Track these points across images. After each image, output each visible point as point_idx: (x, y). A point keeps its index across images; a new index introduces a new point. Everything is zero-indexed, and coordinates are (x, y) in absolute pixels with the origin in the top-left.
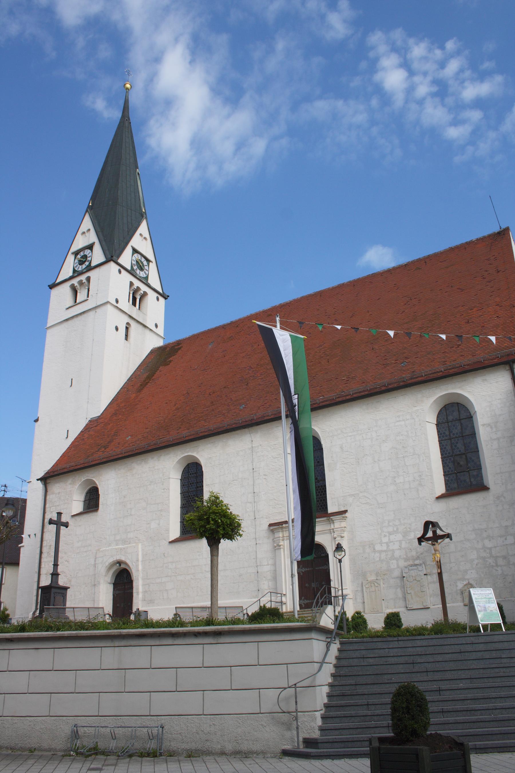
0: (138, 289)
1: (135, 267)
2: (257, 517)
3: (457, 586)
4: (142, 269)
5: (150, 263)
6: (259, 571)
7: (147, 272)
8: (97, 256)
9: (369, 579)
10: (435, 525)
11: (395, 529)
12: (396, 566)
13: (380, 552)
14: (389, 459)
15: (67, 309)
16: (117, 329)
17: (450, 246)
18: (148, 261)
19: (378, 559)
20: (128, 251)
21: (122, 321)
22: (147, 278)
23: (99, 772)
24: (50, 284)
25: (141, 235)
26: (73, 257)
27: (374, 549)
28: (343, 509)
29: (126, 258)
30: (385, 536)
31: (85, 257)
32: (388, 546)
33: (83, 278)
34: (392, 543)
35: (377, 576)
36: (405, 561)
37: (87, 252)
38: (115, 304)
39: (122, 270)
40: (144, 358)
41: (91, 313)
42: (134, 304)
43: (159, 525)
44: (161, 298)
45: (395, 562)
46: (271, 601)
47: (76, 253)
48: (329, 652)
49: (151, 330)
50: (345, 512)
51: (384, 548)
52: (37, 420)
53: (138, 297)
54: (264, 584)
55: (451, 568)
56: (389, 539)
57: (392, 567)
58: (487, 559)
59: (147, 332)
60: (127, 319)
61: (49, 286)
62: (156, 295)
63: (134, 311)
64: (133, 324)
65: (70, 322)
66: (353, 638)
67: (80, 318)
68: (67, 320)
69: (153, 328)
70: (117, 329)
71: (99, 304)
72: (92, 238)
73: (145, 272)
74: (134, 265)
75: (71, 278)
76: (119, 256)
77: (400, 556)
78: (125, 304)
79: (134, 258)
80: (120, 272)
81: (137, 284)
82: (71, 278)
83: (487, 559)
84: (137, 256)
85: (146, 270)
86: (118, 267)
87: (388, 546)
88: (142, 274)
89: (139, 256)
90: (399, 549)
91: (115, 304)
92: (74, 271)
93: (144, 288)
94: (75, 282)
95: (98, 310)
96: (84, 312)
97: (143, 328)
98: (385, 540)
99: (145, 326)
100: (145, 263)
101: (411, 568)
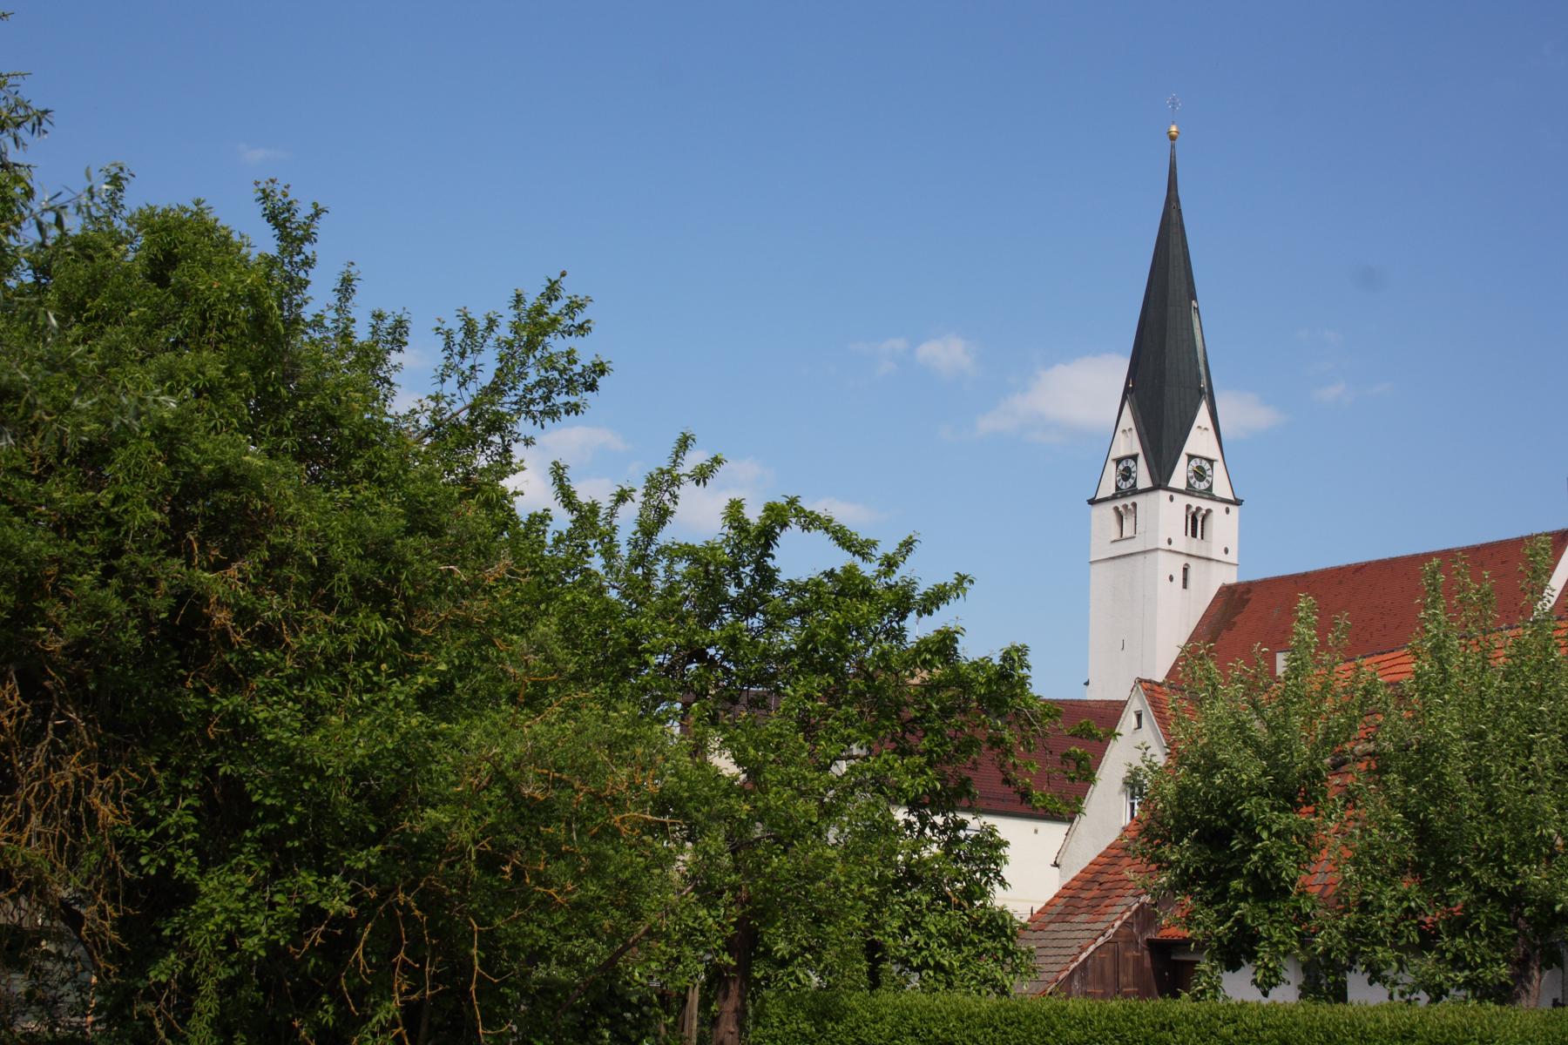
0: (1198, 509)
8: (1143, 479)
16: (1171, 578)
20: (1183, 459)
21: (1176, 565)
23: (568, 473)
26: (1114, 465)
29: (1179, 479)
31: (1127, 469)
33: (1128, 501)
37: (1131, 463)
38: (1167, 547)
41: (1140, 557)
42: (1194, 535)
44: (1232, 508)
47: (1118, 461)
48: (355, 298)
63: (1195, 546)
64: (1193, 563)
66: (1083, 949)
67: (1128, 560)
69: (1222, 557)
70: (1171, 578)
72: (1136, 448)
75: (1114, 497)
76: (1168, 480)
78: (1182, 542)
82: (1114, 497)
92: (1117, 488)
93: (1205, 504)
94: (1119, 504)
95: (1149, 556)
99: (1209, 559)
100: (1206, 466)
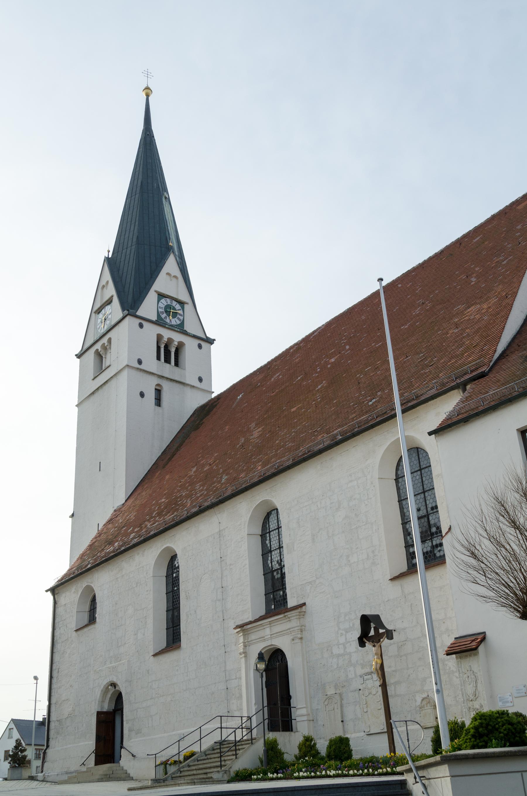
0: (170, 341)
1: (163, 316)
2: (225, 618)
3: (416, 701)
4: (175, 315)
5: (186, 306)
6: (228, 687)
7: (181, 318)
9: (328, 693)
10: (377, 618)
11: (351, 625)
12: (353, 675)
13: (339, 656)
14: (343, 532)
15: (93, 379)
16: (142, 395)
17: (492, 214)
18: (182, 303)
19: (335, 667)
22: (182, 324)
24: (77, 353)
25: (168, 274)
27: (332, 653)
28: (302, 602)
29: (149, 307)
30: (342, 634)
32: (345, 648)
34: (349, 644)
35: (336, 689)
36: (362, 668)
39: (144, 323)
40: (184, 423)
43: (144, 635)
45: (352, 669)
46: (221, 728)
49: (193, 387)
50: (304, 604)
51: (342, 651)
52: (73, 515)
53: (173, 350)
54: (233, 703)
55: (409, 676)
56: (346, 639)
57: (350, 676)
58: (446, 662)
59: (188, 390)
60: (155, 381)
61: (76, 355)
62: (198, 342)
65: (96, 395)
68: (93, 393)
69: (197, 384)
70: (142, 395)
71: (119, 369)
73: (179, 319)
74: (163, 313)
77: (357, 661)
79: (160, 305)
80: (141, 326)
81: (167, 334)
83: (446, 662)
84: (164, 302)
85: (180, 315)
86: (139, 321)
87: (345, 648)
88: (175, 322)
89: (168, 300)
90: (355, 652)
91: (137, 366)
93: (177, 338)
96: (106, 382)
97: (181, 386)
98: (342, 640)
100: (178, 307)
101: (365, 677)
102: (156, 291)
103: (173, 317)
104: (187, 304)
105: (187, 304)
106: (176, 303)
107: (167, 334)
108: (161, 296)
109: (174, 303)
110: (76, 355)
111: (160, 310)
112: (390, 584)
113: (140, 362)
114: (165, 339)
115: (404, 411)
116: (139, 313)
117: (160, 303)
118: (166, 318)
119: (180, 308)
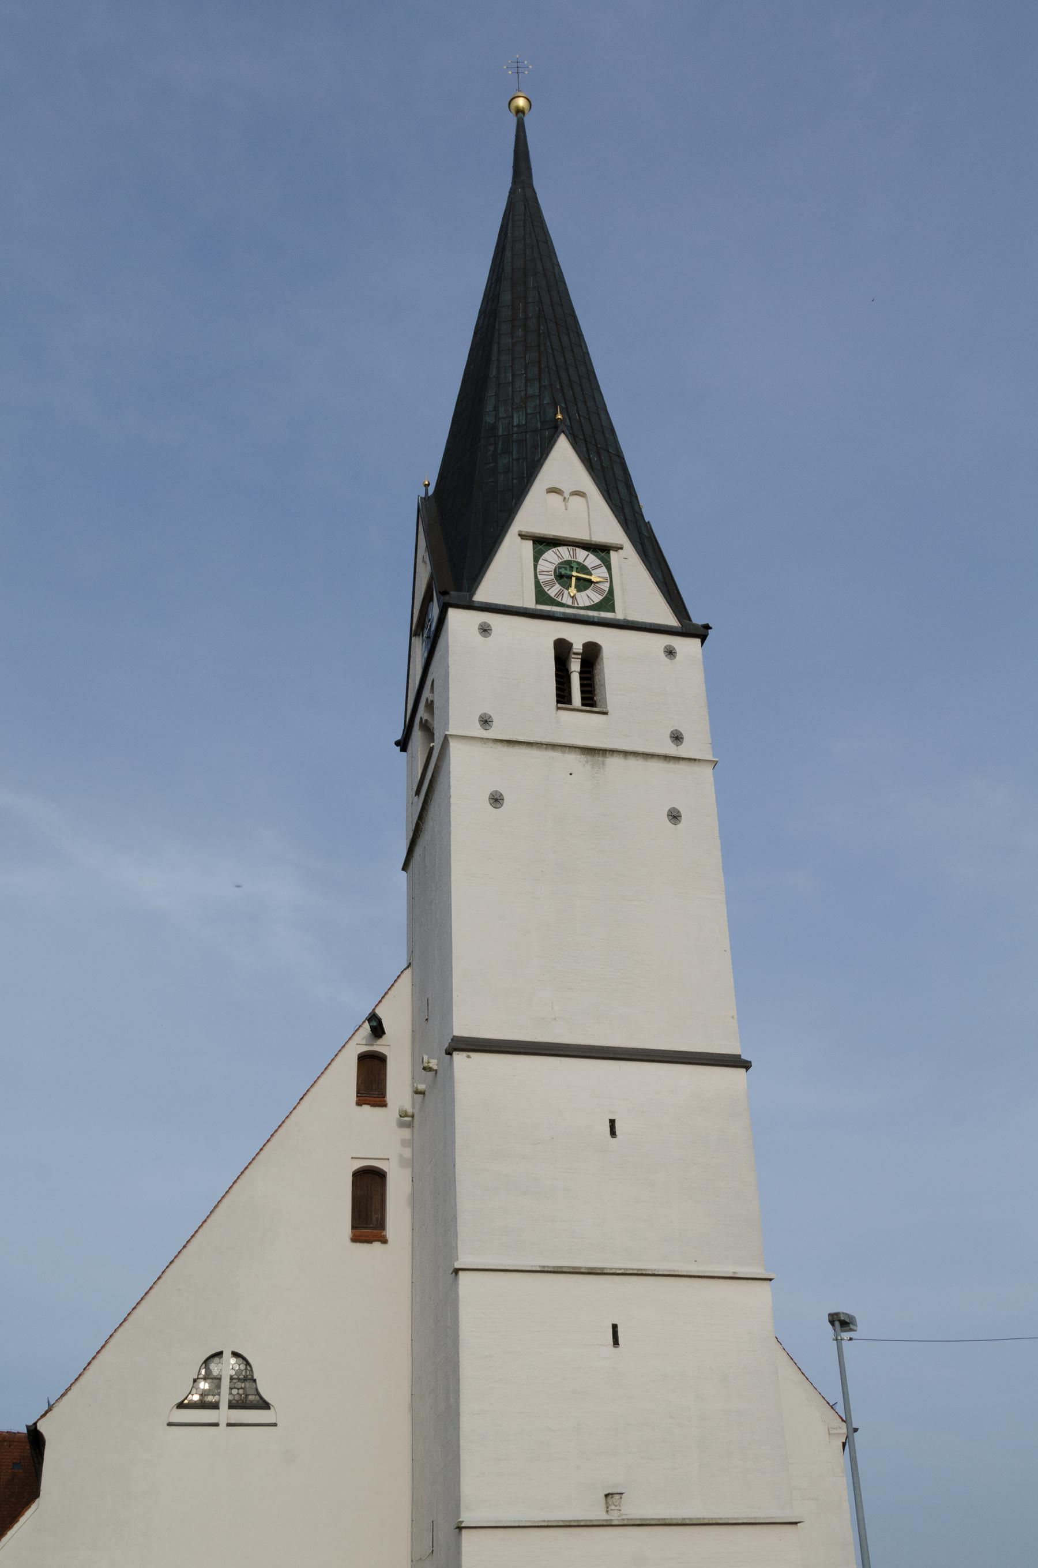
1: (553, 591)
4: (584, 584)
79: (543, 565)
84: (552, 558)
91: (480, 732)
100: (591, 560)
102: (523, 536)
103: (579, 589)
104: (618, 548)
105: (618, 548)
106: (584, 553)
107: (578, 636)
108: (543, 543)
109: (581, 555)
110: (397, 743)
111: (542, 578)
112: (175, 1410)
113: (486, 722)
114: (578, 647)
115: (614, 611)
116: (481, 595)
117: (541, 562)
118: (560, 593)
119: (599, 562)
